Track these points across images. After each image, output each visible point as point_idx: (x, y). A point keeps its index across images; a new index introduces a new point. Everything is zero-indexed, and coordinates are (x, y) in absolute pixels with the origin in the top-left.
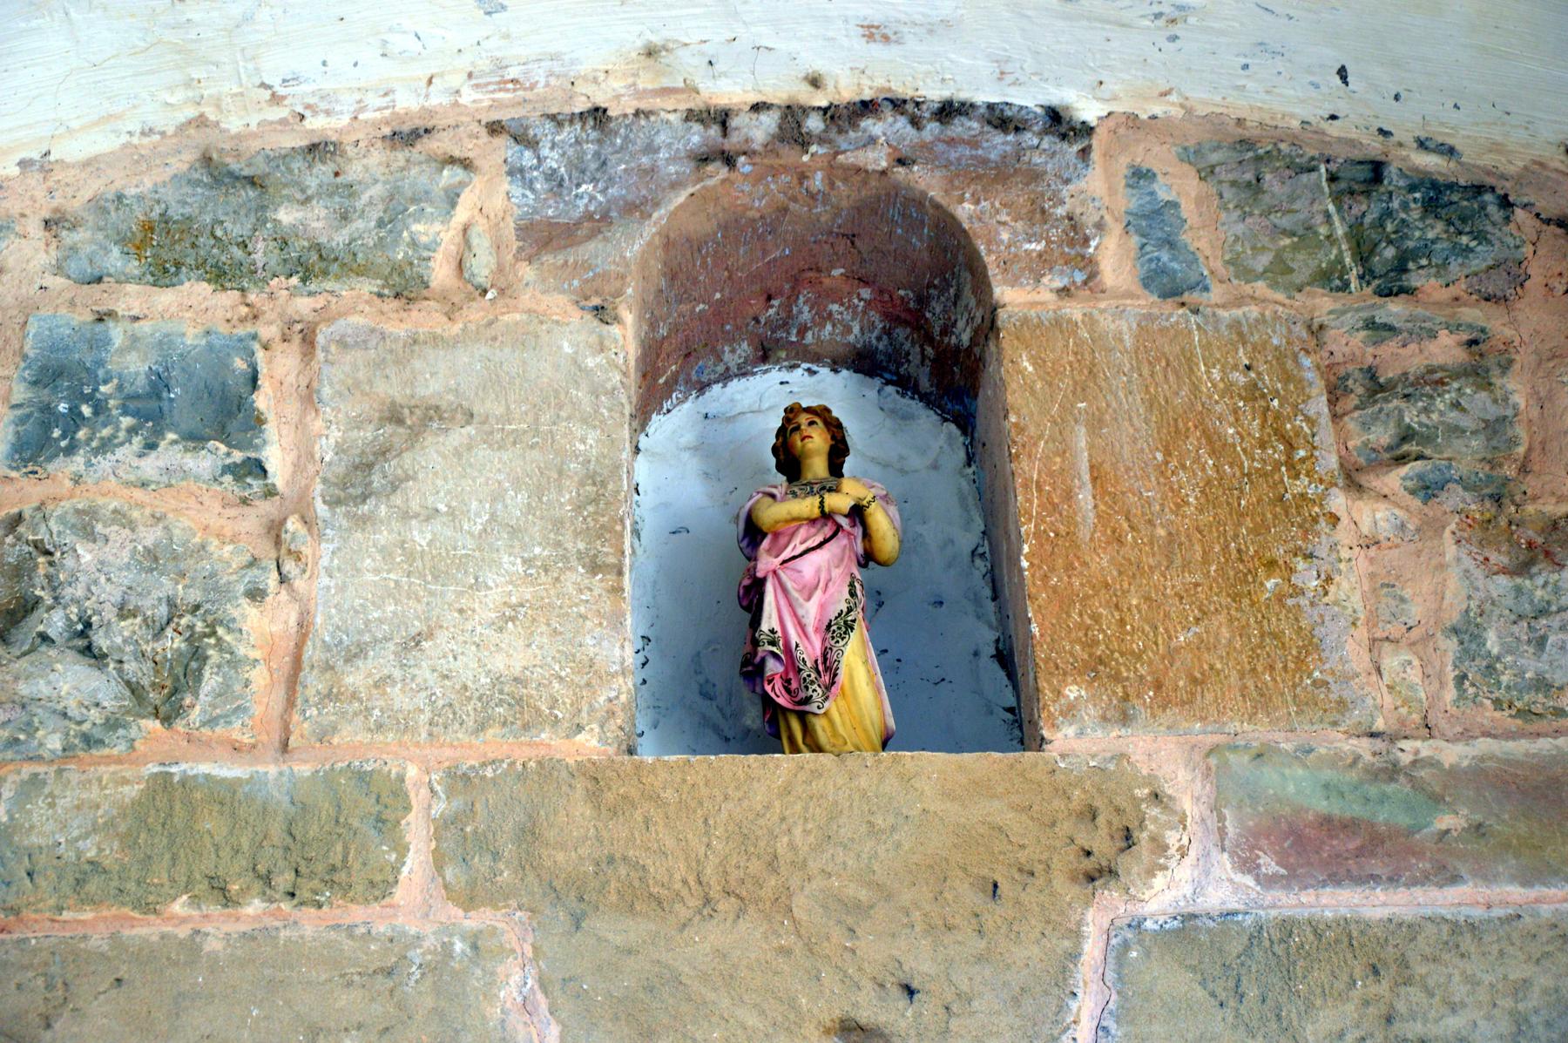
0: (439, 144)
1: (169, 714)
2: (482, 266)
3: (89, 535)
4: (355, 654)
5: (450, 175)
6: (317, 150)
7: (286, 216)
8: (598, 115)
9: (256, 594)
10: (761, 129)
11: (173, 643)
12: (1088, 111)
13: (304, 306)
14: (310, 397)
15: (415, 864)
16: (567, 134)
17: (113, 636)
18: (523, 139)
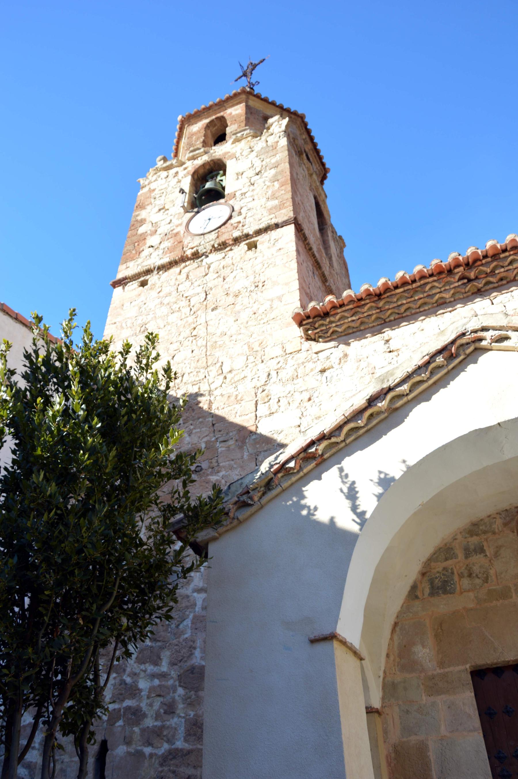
0: (492, 516)
1: (487, 582)
2: (500, 529)
3: (474, 566)
4: (502, 573)
5: (495, 520)
6: (481, 520)
7: (481, 528)
8: (506, 510)
9: (491, 569)
11: (485, 575)
13: (485, 537)
14: (489, 547)
15: (514, 595)
16: (504, 512)
17: (480, 575)
18: (500, 514)
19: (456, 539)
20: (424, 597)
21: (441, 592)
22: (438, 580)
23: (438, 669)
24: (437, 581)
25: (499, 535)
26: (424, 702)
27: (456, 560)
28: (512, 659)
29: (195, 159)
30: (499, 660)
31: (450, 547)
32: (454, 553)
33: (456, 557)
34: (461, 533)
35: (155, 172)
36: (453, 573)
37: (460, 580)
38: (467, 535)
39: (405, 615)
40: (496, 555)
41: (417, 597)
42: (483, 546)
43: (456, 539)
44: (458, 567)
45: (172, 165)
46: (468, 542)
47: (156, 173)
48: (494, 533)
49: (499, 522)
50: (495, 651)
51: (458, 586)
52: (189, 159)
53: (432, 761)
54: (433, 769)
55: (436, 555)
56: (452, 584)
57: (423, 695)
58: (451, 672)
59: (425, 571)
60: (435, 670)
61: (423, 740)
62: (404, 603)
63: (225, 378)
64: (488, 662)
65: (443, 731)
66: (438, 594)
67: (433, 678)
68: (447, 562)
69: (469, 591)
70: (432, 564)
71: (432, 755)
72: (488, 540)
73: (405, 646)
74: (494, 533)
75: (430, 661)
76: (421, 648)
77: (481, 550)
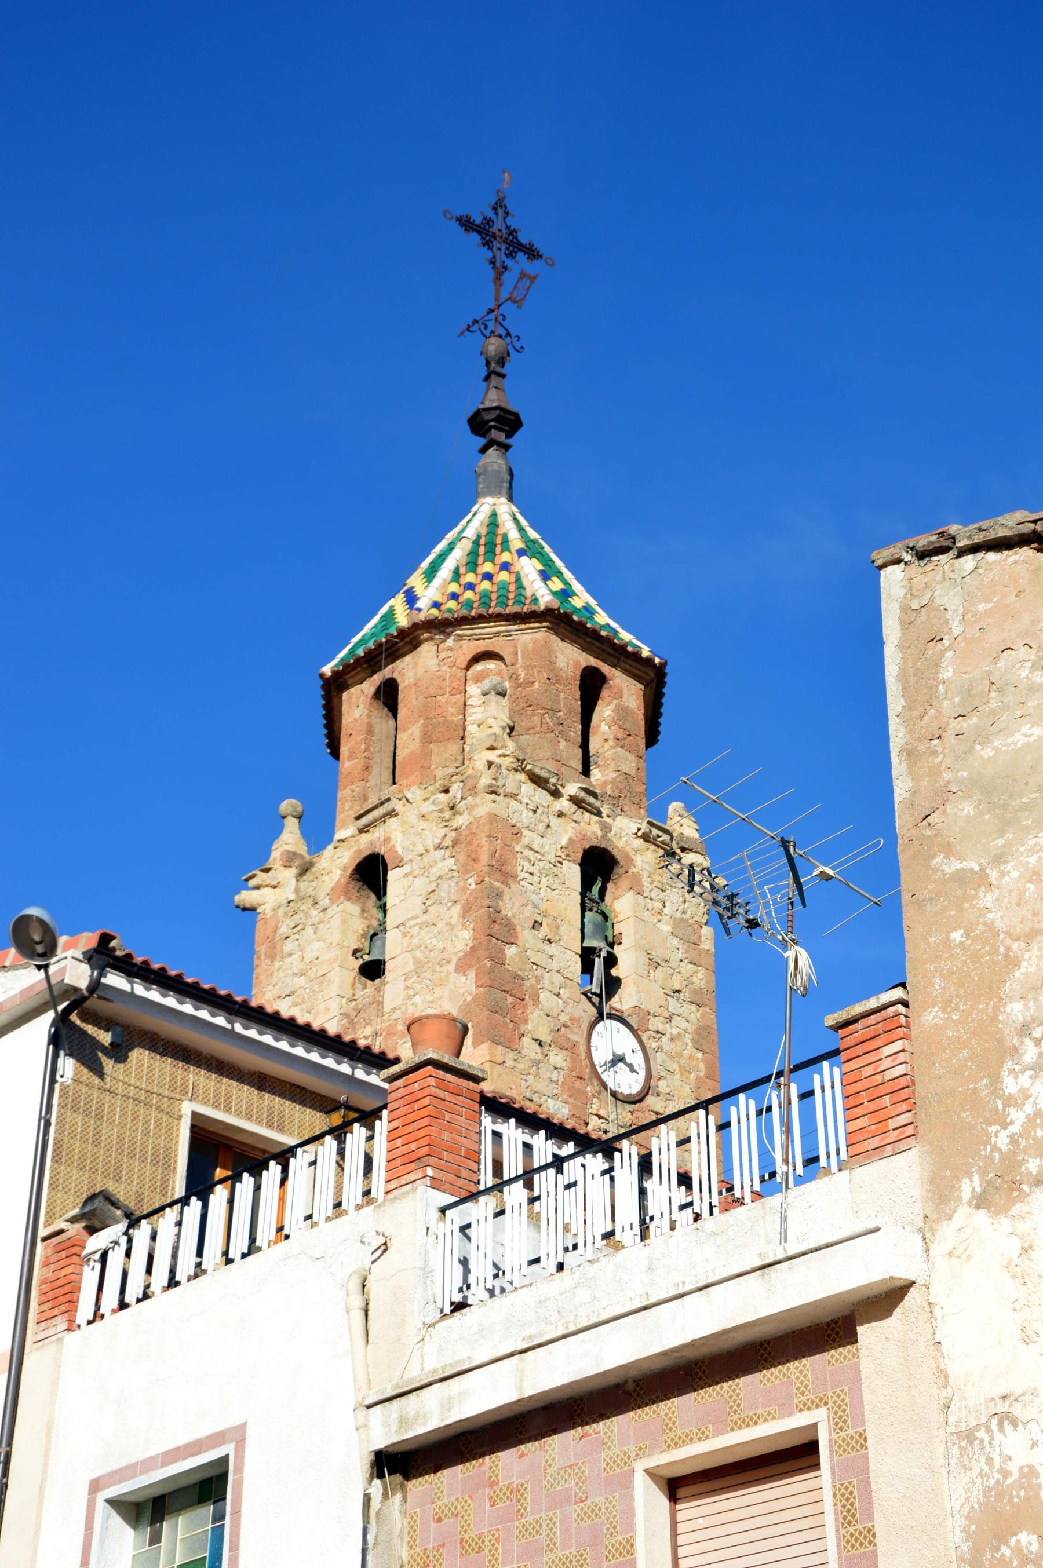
29: (580, 807)
35: (515, 765)
45: (547, 781)
47: (516, 770)
52: (573, 799)
63: (685, 1180)
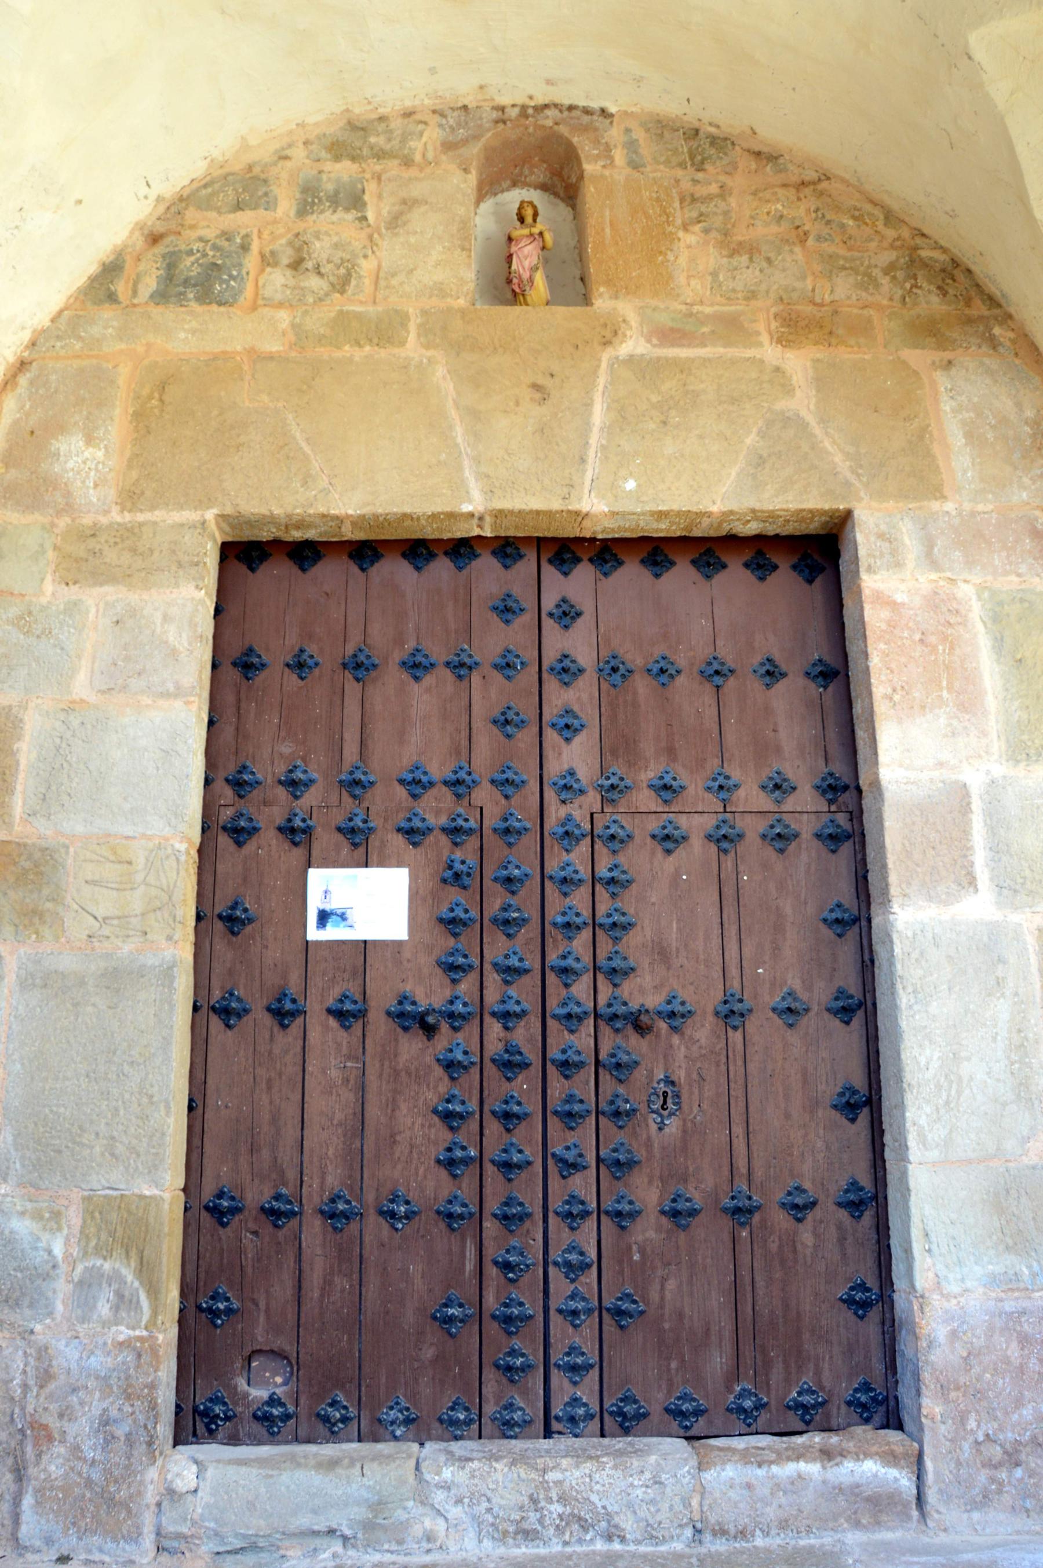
1: (342, 292)
2: (430, 155)
3: (318, 238)
4: (394, 275)
5: (421, 127)
6: (382, 119)
7: (372, 140)
8: (465, 108)
9: (365, 257)
10: (514, 113)
12: (613, 109)
13: (378, 168)
14: (380, 197)
15: (412, 337)
16: (456, 114)
18: (443, 115)
19: (286, 158)
20: (136, 301)
21: (191, 296)
22: (192, 259)
23: (115, 511)
24: (189, 260)
25: (421, 170)
26: (44, 601)
27: (269, 215)
28: (350, 512)
30: (311, 511)
31: (263, 176)
32: (266, 194)
33: (270, 204)
34: (306, 143)
36: (245, 248)
37: (262, 271)
38: (323, 154)
39: (58, 344)
40: (395, 222)
41: (112, 298)
42: (363, 191)
43: (286, 158)
44: (266, 235)
46: (320, 172)
48: (407, 162)
49: (432, 135)
50: (305, 483)
51: (250, 287)
53: (22, 767)
54: (19, 788)
55: (209, 190)
56: (232, 277)
57: (49, 578)
58: (155, 523)
59: (162, 230)
60: (106, 512)
61: (10, 707)
62: (66, 308)
64: (277, 511)
65: (81, 687)
66: (181, 299)
67: (93, 535)
68: (239, 213)
69: (280, 305)
70: (191, 215)
71: (26, 752)
72: (383, 178)
73: (32, 432)
74: (407, 162)
75: (96, 486)
76: (81, 443)
77: (355, 201)
